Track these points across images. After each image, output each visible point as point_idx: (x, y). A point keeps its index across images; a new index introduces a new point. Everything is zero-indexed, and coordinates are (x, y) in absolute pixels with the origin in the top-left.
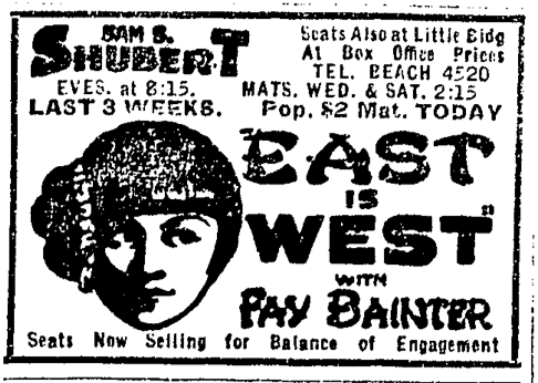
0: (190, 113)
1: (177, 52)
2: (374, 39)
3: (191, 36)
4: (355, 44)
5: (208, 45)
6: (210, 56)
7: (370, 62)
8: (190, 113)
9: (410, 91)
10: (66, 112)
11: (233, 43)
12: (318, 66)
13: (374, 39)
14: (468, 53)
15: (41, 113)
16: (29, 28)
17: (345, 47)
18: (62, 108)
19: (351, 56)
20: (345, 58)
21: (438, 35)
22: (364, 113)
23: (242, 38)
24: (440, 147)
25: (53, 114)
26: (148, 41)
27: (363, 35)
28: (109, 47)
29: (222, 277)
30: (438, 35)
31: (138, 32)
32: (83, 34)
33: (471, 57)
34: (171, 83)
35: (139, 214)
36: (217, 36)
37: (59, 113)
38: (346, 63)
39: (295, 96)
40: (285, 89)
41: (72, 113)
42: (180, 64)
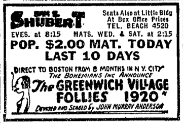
1: (61, 19)
3: (65, 13)
4: (122, 17)
5: (71, 17)
6: (72, 21)
7: (127, 22)
9: (137, 34)
10: (63, 59)
11: (79, 16)
12: (109, 24)
13: (128, 15)
14: (156, 18)
15: (51, 59)
16: (10, 11)
17: (119, 17)
18: (61, 57)
19: (121, 21)
20: (119, 21)
22: (92, 46)
23: (82, 15)
24: (74, 58)
25: (57, 60)
26: (51, 16)
28: (37, 19)
30: (150, 13)
31: (47, 13)
32: (28, 13)
33: (157, 20)
34: (166, 32)
36: (74, 14)
37: (59, 59)
38: (119, 23)
39: (142, 36)
40: (25, 34)
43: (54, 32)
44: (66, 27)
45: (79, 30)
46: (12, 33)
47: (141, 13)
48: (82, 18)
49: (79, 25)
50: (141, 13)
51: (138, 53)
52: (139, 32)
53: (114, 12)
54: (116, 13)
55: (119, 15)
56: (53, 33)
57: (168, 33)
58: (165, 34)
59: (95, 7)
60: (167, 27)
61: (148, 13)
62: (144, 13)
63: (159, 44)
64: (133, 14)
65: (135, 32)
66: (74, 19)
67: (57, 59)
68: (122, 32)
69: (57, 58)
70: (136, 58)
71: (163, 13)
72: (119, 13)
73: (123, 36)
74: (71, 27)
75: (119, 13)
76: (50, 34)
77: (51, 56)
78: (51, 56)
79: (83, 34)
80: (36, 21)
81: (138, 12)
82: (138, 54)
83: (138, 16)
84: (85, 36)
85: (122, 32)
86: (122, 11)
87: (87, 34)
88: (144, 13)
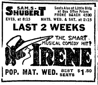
0: (75, 29)
2: (68, 9)
8: (75, 29)
11: (43, 9)
14: (82, 11)
15: (17, 30)
16: (6, 5)
18: (25, 28)
21: (80, 8)
23: (44, 8)
27: (66, 8)
29: (32, 66)
35: (15, 51)
37: (24, 30)
41: (70, 36)
42: (33, 13)
43: (27, 18)
44: (35, 15)
45: (42, 17)
46: (6, 18)
47: (75, 8)
48: (44, 11)
49: (42, 14)
50: (75, 8)
51: (84, 25)
52: (74, 19)
53: (61, 7)
54: (61, 8)
55: (63, 9)
56: (27, 19)
57: (28, 19)
58: (87, 20)
59: (48, 4)
60: (91, 16)
61: (79, 8)
62: (77, 8)
63: (22, 27)
64: (71, 8)
65: (72, 19)
66: (40, 11)
67: (22, 30)
68: (66, 19)
69: (22, 28)
70: (82, 26)
71: (87, 8)
72: (63, 8)
73: (66, 20)
74: (38, 15)
75: (63, 8)
76: (25, 19)
77: (17, 27)
78: (17, 27)
79: (46, 19)
80: (24, 13)
81: (74, 8)
82: (84, 27)
83: (73, 10)
84: (47, 20)
85: (66, 19)
86: (65, 7)
87: (48, 19)
88: (77, 8)
